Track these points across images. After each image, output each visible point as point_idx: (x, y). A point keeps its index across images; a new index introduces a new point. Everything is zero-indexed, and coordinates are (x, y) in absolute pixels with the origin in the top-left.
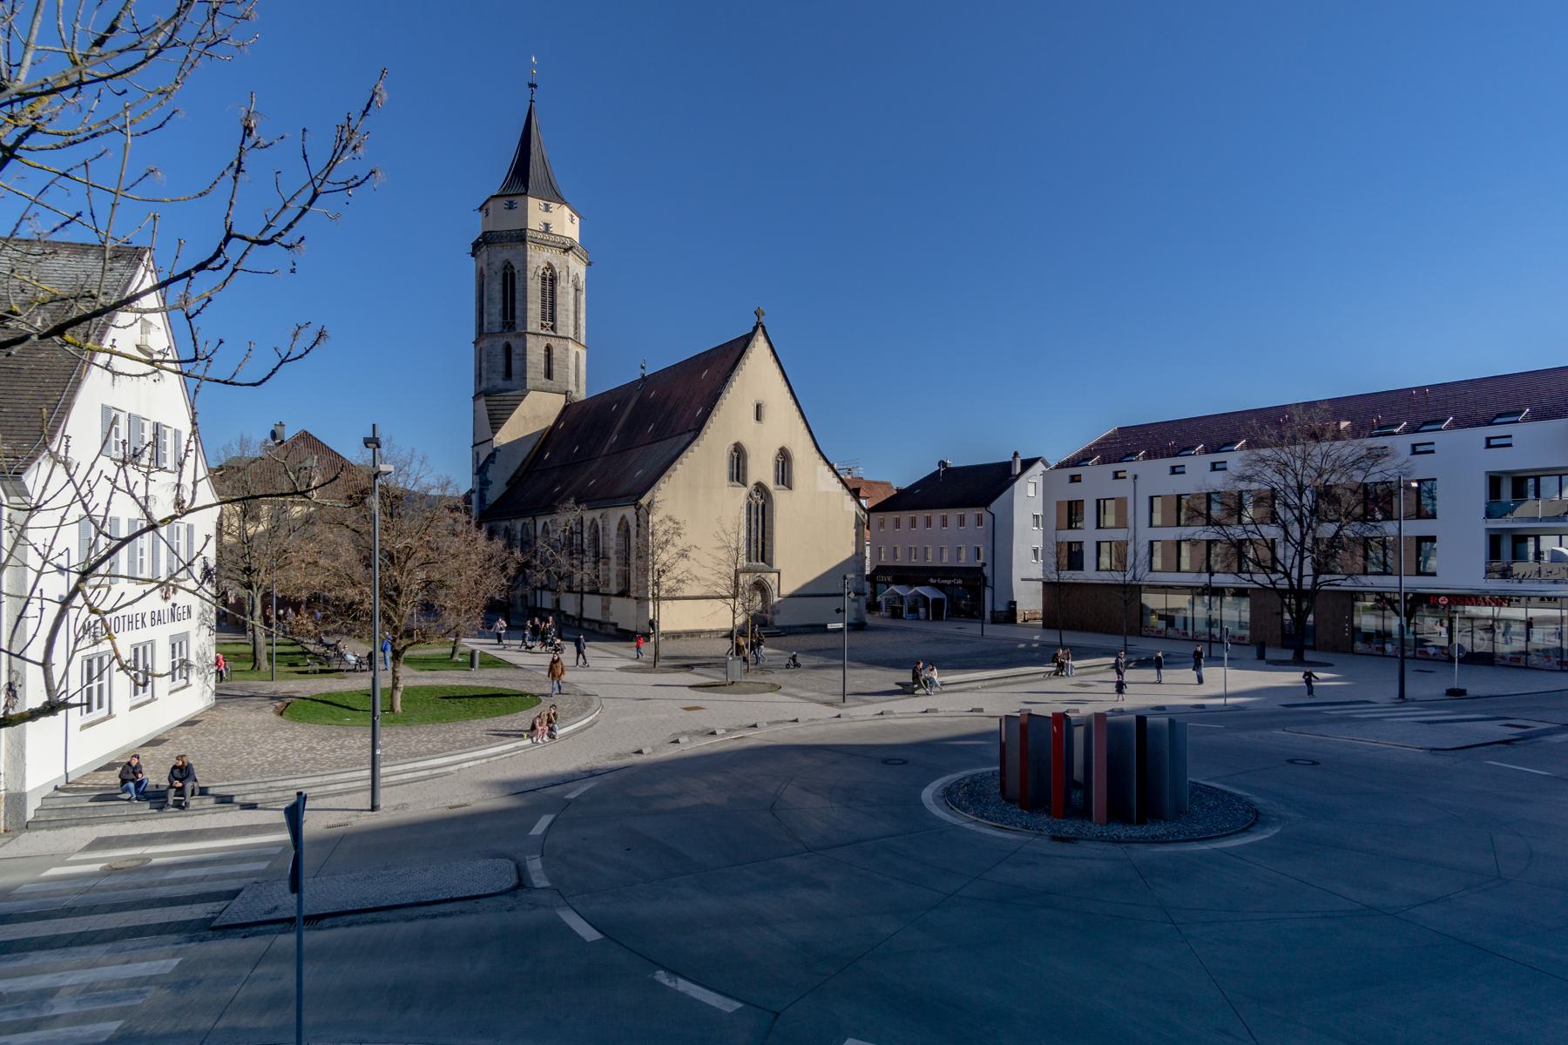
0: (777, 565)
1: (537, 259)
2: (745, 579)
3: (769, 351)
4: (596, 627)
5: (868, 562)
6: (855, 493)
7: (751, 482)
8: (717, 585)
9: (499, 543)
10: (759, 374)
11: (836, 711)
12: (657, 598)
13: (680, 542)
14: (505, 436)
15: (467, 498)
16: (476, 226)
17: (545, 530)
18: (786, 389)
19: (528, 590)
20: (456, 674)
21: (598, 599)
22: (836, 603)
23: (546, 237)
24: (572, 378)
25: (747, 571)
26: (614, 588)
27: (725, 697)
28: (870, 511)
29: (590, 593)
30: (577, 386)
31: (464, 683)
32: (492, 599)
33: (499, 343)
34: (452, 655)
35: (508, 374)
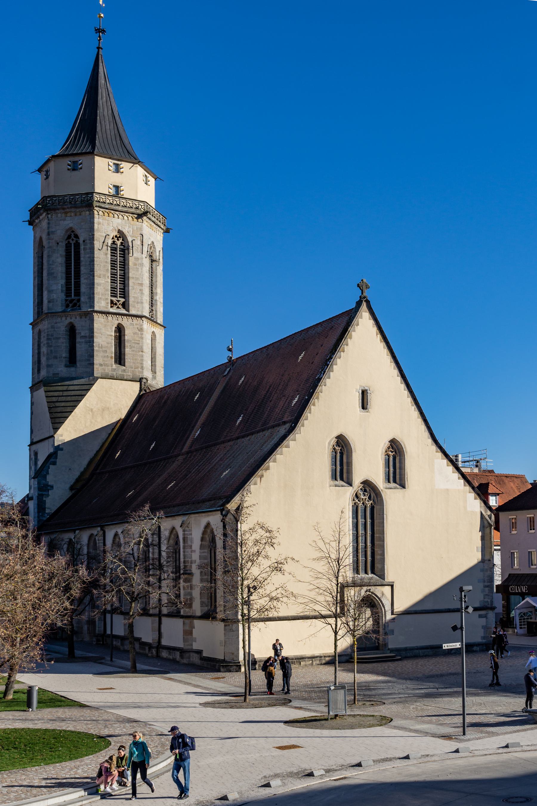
0: (390, 577)
1: (106, 226)
2: (352, 595)
3: (375, 329)
4: (177, 655)
5: (497, 571)
6: (482, 491)
7: (357, 480)
8: (316, 602)
9: (61, 560)
10: (363, 356)
11: (453, 745)
12: (248, 620)
13: (274, 554)
14: (68, 432)
15: (24, 502)
16: (34, 191)
17: (117, 544)
18: (396, 372)
19: (96, 614)
20: (10, 715)
21: (178, 623)
22: (453, 619)
23: (117, 201)
24: (148, 363)
25: (354, 584)
26: (197, 609)
27: (326, 732)
28: (501, 509)
29: (170, 615)
30: (154, 371)
31: (19, 725)
32: (52, 626)
33: (62, 324)
34: (5, 693)
35: (72, 360)
